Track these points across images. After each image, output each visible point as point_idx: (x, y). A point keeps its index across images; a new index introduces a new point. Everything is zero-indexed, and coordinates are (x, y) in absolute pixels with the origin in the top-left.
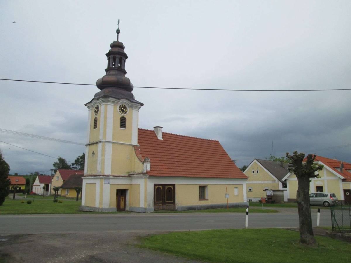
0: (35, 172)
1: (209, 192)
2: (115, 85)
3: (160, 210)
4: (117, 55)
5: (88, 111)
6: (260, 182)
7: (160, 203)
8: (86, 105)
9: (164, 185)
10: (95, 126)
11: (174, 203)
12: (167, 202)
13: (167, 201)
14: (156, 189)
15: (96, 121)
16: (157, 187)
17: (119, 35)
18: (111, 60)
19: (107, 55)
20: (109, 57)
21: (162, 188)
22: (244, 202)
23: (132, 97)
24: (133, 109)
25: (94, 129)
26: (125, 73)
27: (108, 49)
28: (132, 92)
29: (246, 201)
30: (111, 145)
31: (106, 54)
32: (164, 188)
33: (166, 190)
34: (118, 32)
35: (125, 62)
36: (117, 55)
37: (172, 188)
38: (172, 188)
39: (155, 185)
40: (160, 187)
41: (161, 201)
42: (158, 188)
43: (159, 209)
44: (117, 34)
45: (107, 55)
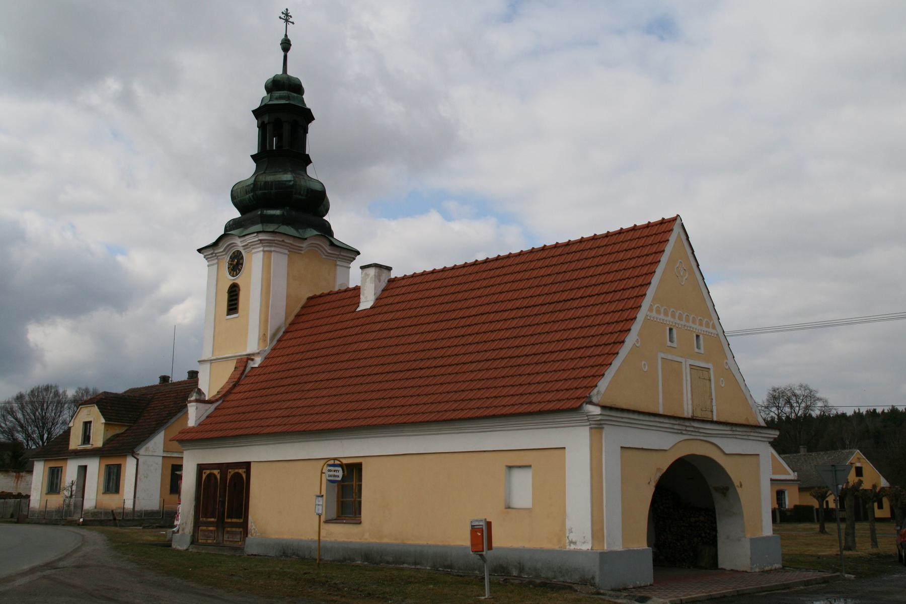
3: (210, 545)
4: (284, 118)
5: (207, 268)
6: (661, 401)
8: (200, 251)
9: (224, 467)
10: (233, 306)
11: (245, 525)
12: (229, 520)
13: (228, 517)
14: (204, 476)
15: (234, 293)
16: (208, 472)
17: (289, 54)
18: (269, 129)
19: (257, 113)
22: (573, 547)
23: (326, 231)
24: (338, 263)
25: (228, 314)
26: (307, 160)
27: (258, 95)
29: (587, 547)
33: (229, 477)
34: (286, 45)
37: (244, 476)
38: (244, 476)
40: (216, 472)
42: (210, 476)
43: (209, 541)
44: (282, 54)
45: (257, 113)
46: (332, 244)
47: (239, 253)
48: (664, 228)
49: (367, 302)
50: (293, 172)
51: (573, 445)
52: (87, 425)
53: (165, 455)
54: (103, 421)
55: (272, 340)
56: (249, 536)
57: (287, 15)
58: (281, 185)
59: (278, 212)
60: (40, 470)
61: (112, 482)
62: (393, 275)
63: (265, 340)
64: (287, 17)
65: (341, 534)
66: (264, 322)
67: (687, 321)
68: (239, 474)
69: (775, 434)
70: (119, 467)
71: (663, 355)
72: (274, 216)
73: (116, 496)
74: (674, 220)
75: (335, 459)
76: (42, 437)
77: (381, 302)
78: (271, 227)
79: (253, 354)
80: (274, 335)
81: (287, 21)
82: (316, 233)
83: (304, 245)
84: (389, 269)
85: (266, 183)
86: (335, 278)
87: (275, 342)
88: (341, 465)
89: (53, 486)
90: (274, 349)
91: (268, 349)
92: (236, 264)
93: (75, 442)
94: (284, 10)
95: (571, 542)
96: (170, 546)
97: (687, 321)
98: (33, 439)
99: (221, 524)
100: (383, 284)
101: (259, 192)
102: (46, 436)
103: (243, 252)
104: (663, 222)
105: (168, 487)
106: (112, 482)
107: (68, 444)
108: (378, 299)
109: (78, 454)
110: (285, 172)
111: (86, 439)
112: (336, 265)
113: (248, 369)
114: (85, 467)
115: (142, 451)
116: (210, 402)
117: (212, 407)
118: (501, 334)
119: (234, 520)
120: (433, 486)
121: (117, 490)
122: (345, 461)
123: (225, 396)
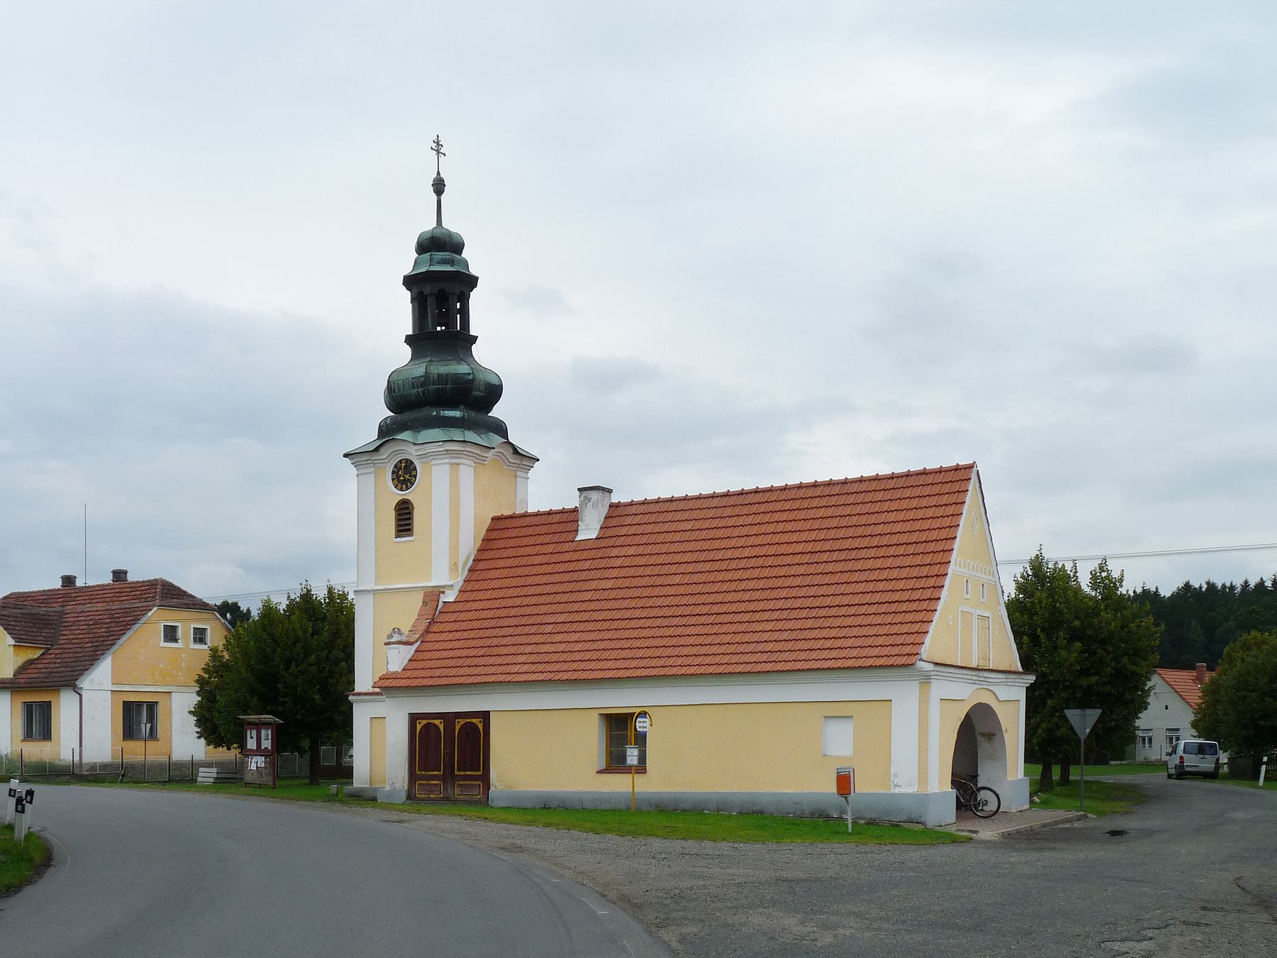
0: (318, 784)
2: (443, 394)
4: (441, 289)
7: (434, 777)
8: (346, 456)
11: (485, 778)
14: (419, 727)
16: (462, 722)
18: (431, 302)
20: (421, 293)
21: (441, 727)
22: (897, 791)
27: (406, 261)
30: (370, 598)
31: (477, 278)
34: (439, 187)
36: (441, 289)
39: (414, 718)
40: (437, 722)
48: (959, 475)
51: (902, 697)
56: (492, 789)
62: (615, 499)
65: (618, 784)
66: (454, 547)
71: (961, 608)
74: (971, 467)
79: (443, 587)
80: (465, 564)
81: (438, 152)
83: (490, 454)
84: (610, 491)
85: (439, 375)
86: (515, 492)
92: (405, 474)
95: (896, 786)
99: (449, 777)
103: (416, 463)
104: (957, 469)
105: (120, 730)
112: (516, 476)
115: (86, 683)
118: (789, 582)
120: (733, 739)
121: (46, 735)
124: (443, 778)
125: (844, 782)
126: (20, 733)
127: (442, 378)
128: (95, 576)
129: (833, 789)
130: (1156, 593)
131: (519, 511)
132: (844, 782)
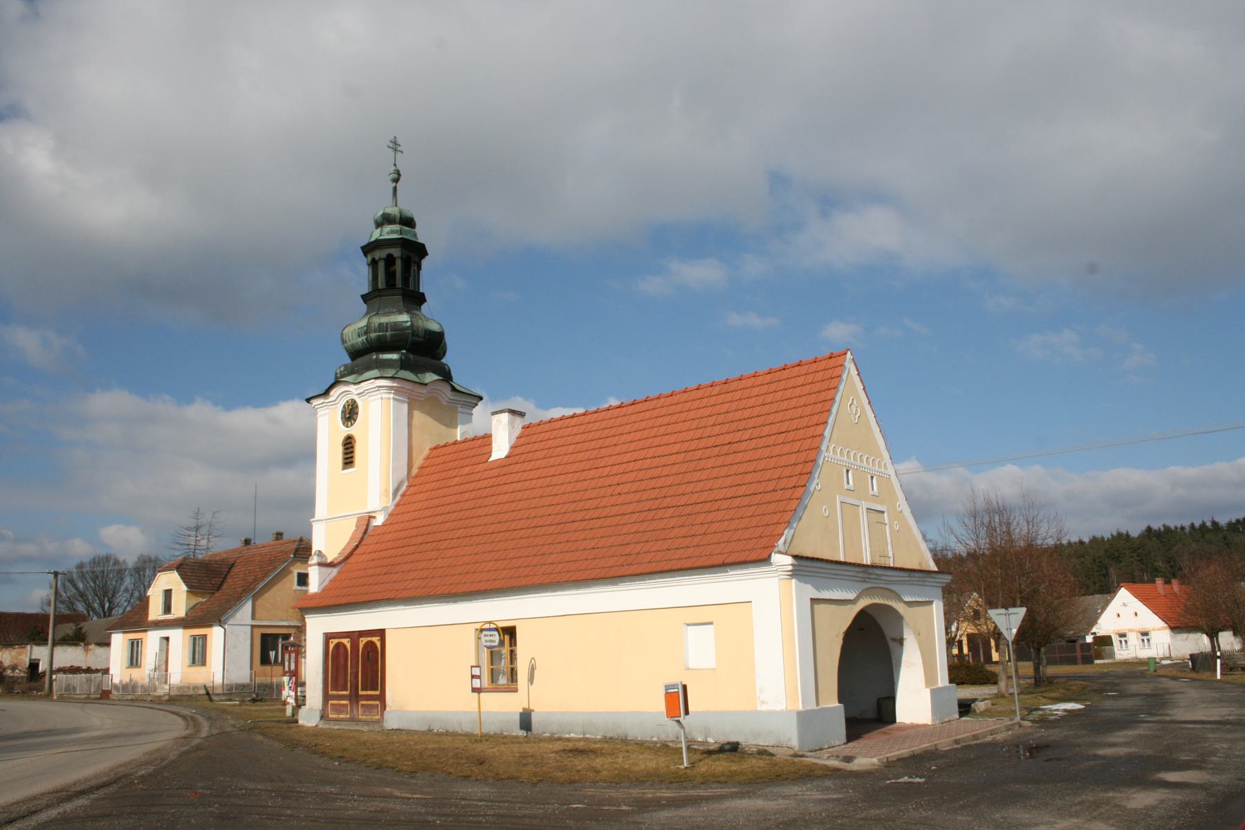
1: (465, 654)
9: (355, 636)
11: (382, 698)
12: (364, 693)
14: (331, 646)
16: (336, 641)
21: (348, 646)
22: (764, 708)
25: (344, 468)
28: (444, 361)
29: (780, 706)
32: (355, 645)
35: (419, 268)
37: (378, 644)
38: (378, 644)
40: (346, 641)
41: (280, 687)
42: (338, 646)
46: (454, 389)
47: (354, 402)
48: (832, 362)
49: (500, 449)
50: (408, 312)
52: (168, 594)
53: (254, 623)
54: (185, 588)
55: (395, 494)
57: (395, 143)
58: (396, 326)
59: (395, 356)
60: (119, 641)
61: (198, 655)
63: (387, 496)
64: (395, 146)
67: (861, 460)
68: (372, 643)
69: (947, 578)
70: (204, 637)
72: (391, 360)
73: (203, 669)
75: (490, 623)
76: (103, 607)
77: (518, 451)
78: (390, 373)
81: (396, 150)
82: (436, 377)
85: (380, 324)
87: (398, 498)
88: (496, 629)
89: (134, 660)
90: (398, 505)
91: (391, 504)
93: (155, 611)
94: (392, 138)
95: (763, 702)
96: (297, 722)
97: (861, 460)
98: (93, 609)
99: (355, 698)
100: (518, 431)
101: (373, 335)
102: (107, 605)
106: (198, 655)
107: (147, 614)
108: (513, 447)
109: (158, 625)
110: (400, 313)
111: (167, 609)
113: (370, 529)
114: (167, 639)
116: (331, 565)
117: (335, 571)
119: (370, 693)
122: (501, 625)
123: (347, 558)
124: (349, 698)
125: (677, 700)
126: (188, 660)
127: (381, 327)
128: (263, 539)
129: (660, 705)
130: (1128, 535)
131: (451, 441)
132: (677, 700)
